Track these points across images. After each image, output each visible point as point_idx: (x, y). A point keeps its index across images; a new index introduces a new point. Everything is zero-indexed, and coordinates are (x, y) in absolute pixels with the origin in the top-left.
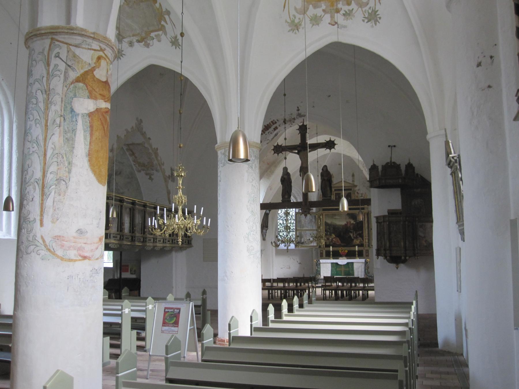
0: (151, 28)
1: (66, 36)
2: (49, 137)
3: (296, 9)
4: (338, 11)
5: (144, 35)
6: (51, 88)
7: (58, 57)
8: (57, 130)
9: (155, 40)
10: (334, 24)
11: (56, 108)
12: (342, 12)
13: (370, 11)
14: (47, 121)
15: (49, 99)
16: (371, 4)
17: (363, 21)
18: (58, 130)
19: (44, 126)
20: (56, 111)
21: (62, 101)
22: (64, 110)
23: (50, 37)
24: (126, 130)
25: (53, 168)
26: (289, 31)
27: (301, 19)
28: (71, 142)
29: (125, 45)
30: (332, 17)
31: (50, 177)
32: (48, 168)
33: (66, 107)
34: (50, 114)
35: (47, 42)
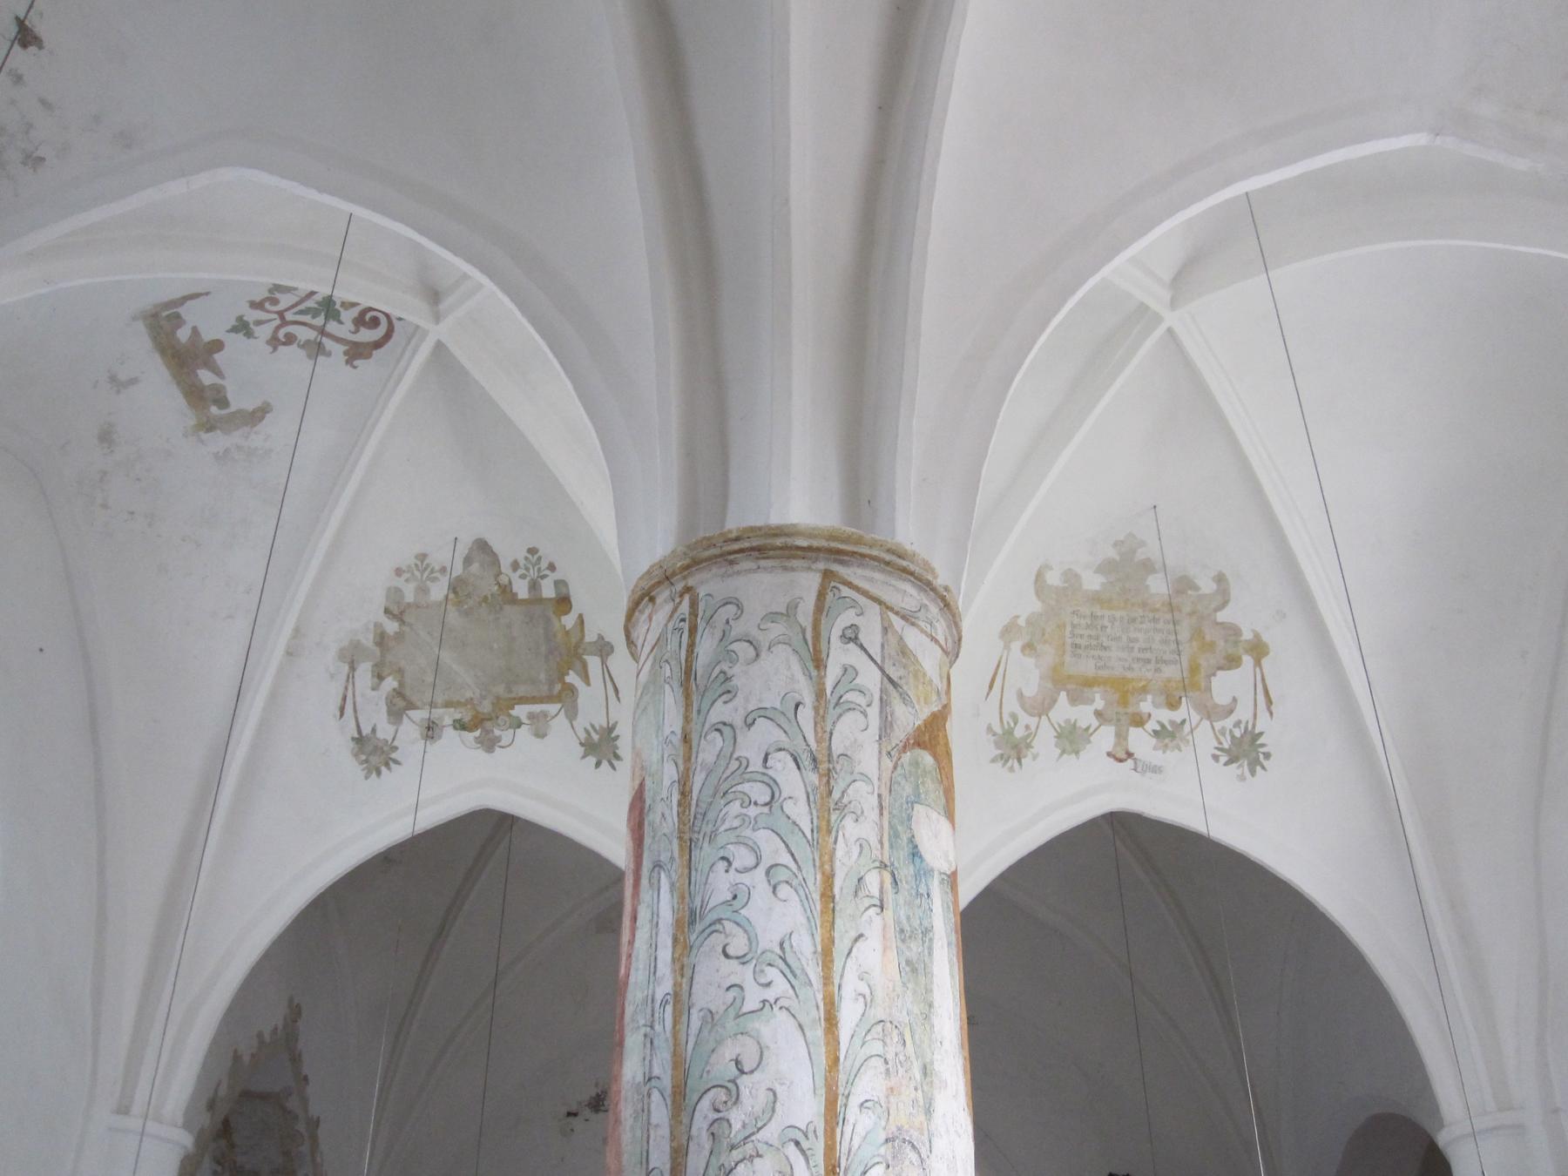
0: (521, 690)
1: (877, 576)
2: (841, 947)
3: (1020, 695)
4: (1139, 721)
5: (486, 707)
6: (837, 748)
7: (854, 640)
8: (874, 925)
9: (524, 732)
10: (1124, 756)
11: (858, 836)
12: (1151, 725)
13: (1237, 733)
14: (829, 880)
15: (830, 793)
16: (1243, 713)
17: (1216, 758)
18: (878, 921)
19: (816, 896)
20: (862, 844)
21: (881, 808)
22: (891, 847)
23: (821, 566)
24: (260, 1035)
25: (868, 1085)
26: (993, 761)
27: (1033, 728)
28: (922, 979)
29: (409, 732)
30: (1121, 737)
31: (859, 1126)
32: (850, 1083)
33: (895, 835)
34: (839, 853)
35: (807, 582)
